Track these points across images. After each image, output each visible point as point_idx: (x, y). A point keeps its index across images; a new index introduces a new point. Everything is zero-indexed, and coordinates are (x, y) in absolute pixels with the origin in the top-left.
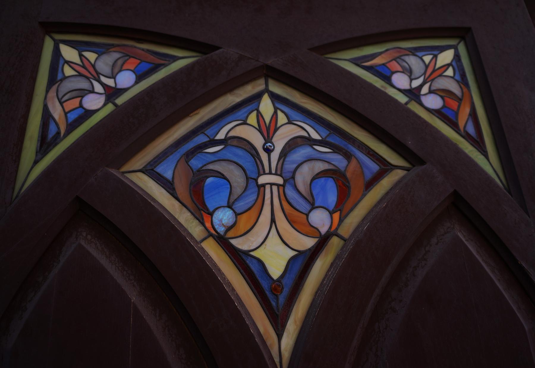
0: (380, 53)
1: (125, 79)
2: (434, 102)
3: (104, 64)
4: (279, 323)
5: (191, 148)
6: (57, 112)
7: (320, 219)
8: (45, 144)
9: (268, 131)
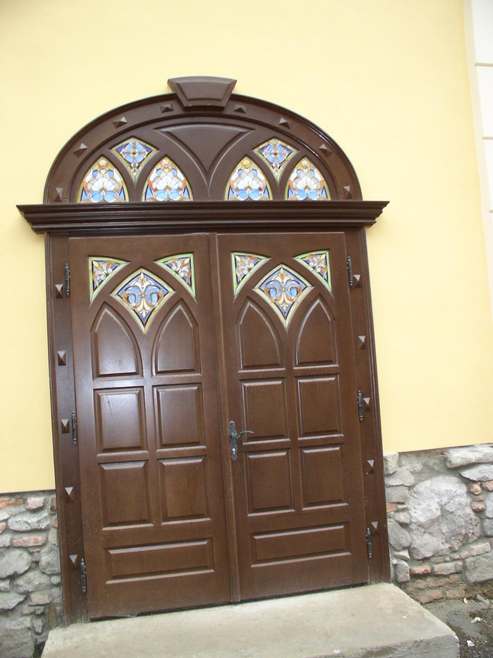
0: (170, 260)
2: (319, 270)
3: (247, 261)
4: (286, 318)
6: (239, 275)
8: (238, 283)
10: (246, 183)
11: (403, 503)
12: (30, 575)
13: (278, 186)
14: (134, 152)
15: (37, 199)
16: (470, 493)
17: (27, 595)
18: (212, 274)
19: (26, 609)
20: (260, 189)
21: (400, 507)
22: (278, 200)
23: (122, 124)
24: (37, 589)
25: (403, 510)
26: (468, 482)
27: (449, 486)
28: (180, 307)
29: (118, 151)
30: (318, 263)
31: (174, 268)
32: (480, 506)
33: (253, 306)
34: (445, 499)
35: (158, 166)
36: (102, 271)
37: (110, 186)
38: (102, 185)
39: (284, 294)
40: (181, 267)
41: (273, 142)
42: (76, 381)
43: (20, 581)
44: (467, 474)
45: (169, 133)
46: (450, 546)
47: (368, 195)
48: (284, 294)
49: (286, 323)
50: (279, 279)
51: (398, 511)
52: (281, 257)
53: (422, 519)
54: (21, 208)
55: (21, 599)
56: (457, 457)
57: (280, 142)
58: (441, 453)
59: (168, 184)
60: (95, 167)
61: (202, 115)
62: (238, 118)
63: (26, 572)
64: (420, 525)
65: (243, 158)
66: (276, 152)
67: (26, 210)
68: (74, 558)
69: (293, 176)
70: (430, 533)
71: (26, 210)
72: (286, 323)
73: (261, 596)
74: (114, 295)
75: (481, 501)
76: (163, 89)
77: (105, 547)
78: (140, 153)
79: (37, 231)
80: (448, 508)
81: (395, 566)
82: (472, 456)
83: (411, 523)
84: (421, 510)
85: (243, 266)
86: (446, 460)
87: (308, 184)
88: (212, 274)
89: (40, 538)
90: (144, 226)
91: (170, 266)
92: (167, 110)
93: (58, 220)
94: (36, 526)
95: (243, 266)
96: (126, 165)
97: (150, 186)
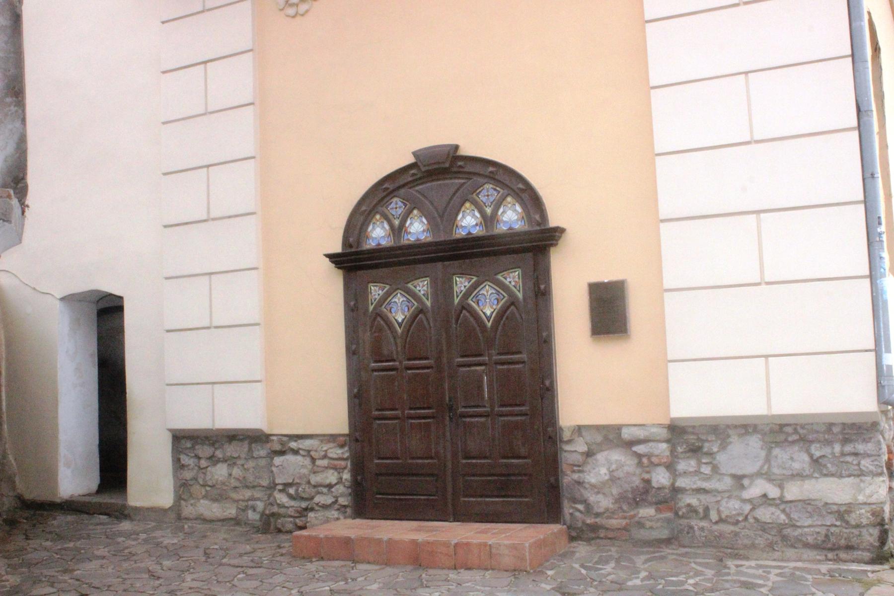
0: (415, 282)
1: (466, 284)
2: (513, 283)
5: (389, 303)
7: (494, 307)
9: (487, 292)
10: (468, 222)
11: (579, 466)
12: (337, 486)
13: (489, 220)
14: (396, 206)
15: (337, 248)
16: (640, 464)
17: (336, 497)
18: (443, 289)
19: (336, 506)
20: (477, 225)
21: (575, 468)
22: (442, 238)
23: (387, 189)
24: (342, 495)
25: (579, 471)
26: (639, 456)
27: (616, 456)
28: (512, 307)
29: (387, 208)
30: (513, 278)
31: (418, 288)
32: (646, 476)
33: (467, 314)
34: (614, 467)
35: (411, 216)
36: (376, 291)
37: (473, 222)
38: (378, 234)
39: (488, 304)
40: (422, 287)
41: (487, 186)
42: (175, 382)
43: (333, 490)
44: (640, 449)
45: (417, 191)
46: (746, 495)
47: (553, 222)
48: (488, 304)
49: (489, 325)
50: (396, 300)
51: (574, 471)
52: (398, 285)
53: (593, 481)
54: (328, 256)
55: (333, 500)
56: (626, 434)
57: (491, 186)
58: (618, 428)
59: (417, 229)
60: (374, 220)
61: (443, 172)
62: (458, 173)
63: (336, 484)
64: (593, 486)
65: (463, 204)
66: (488, 193)
67: (332, 257)
68: (359, 478)
69: (501, 211)
70: (604, 494)
71: (332, 257)
72: (489, 325)
73: (420, 517)
74: (383, 308)
75: (648, 472)
76: (411, 160)
77: (826, 459)
78: (400, 207)
79: (339, 268)
80: (615, 474)
81: (571, 514)
82: (641, 433)
83: (584, 482)
84: (597, 472)
85: (461, 284)
86: (620, 435)
87: (511, 217)
88: (443, 289)
89: (343, 463)
90: (400, 260)
91: (415, 287)
92: (413, 175)
93: (353, 262)
94: (341, 456)
95: (461, 284)
96: (391, 217)
97: (406, 230)
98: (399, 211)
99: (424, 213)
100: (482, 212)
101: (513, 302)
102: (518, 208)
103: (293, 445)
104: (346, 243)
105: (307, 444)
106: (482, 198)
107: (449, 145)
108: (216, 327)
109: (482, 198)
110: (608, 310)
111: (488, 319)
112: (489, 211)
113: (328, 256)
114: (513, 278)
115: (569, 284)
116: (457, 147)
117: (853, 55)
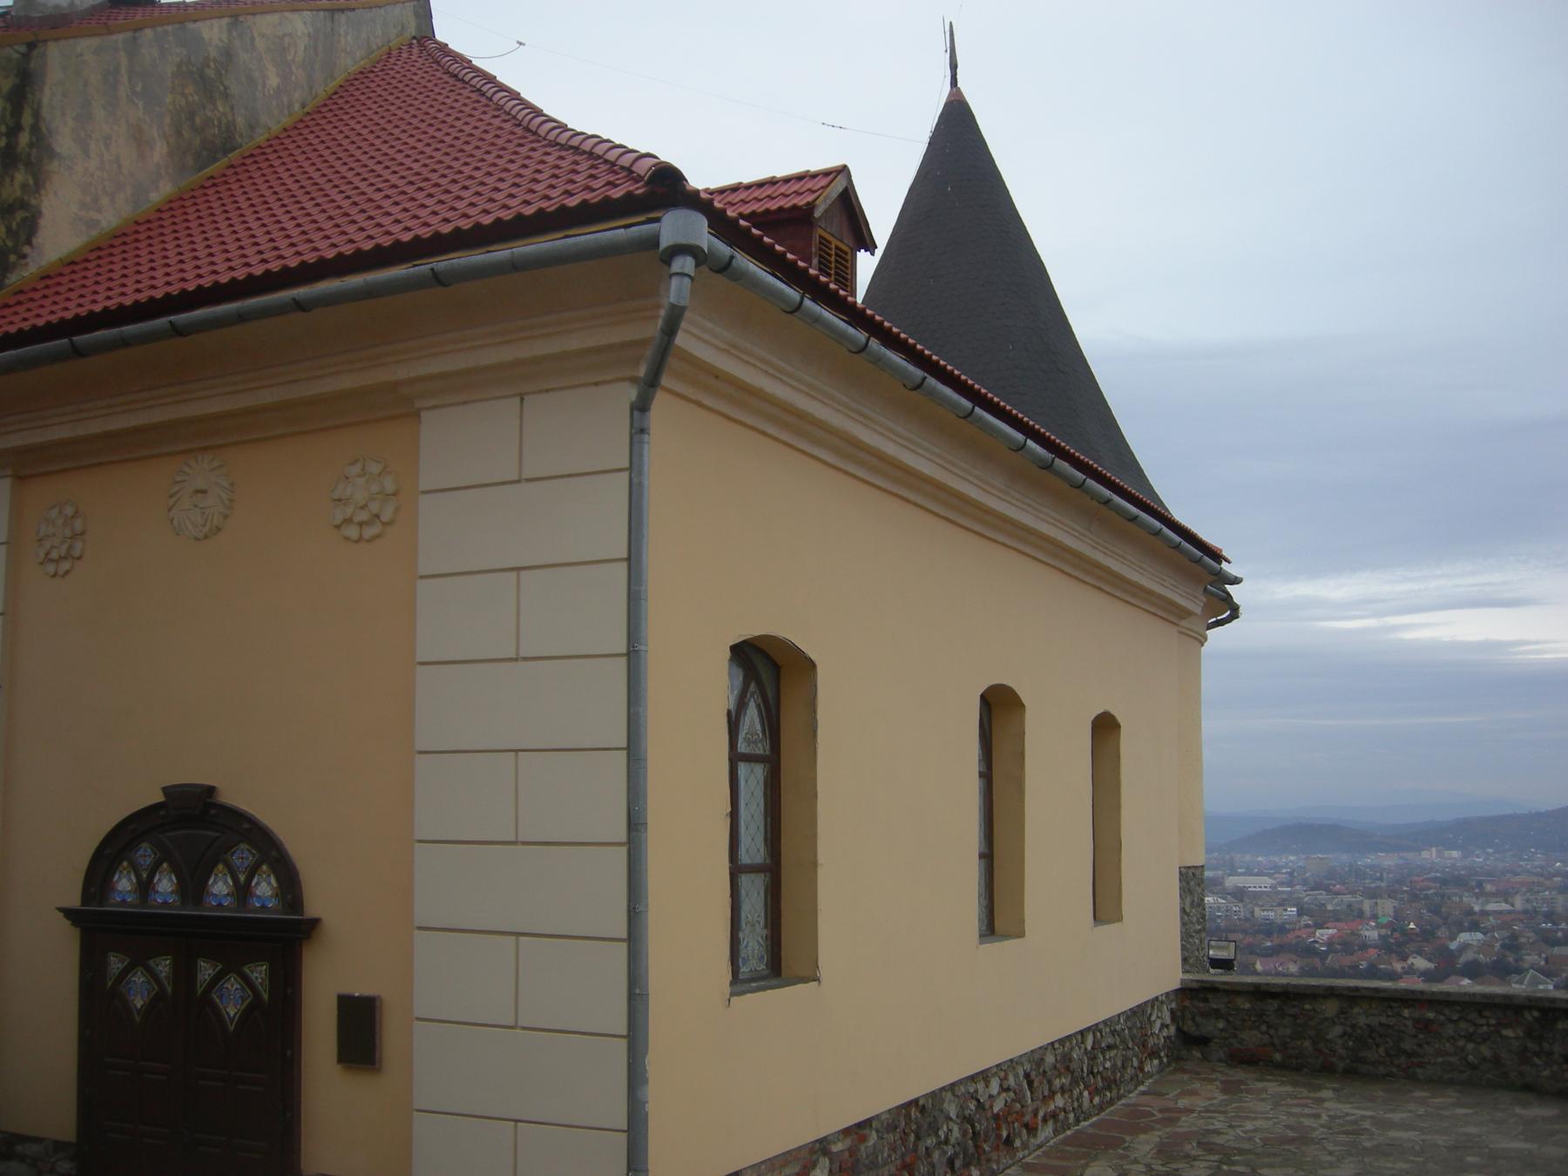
0: (157, 960)
14: (145, 854)
18: (184, 973)
30: (259, 973)
45: (1143, 1093)
49: (232, 1028)
54: (60, 910)
61: (193, 824)
67: (68, 913)
71: (68, 913)
76: (160, 798)
88: (184, 973)
95: (206, 970)
98: (149, 861)
99: (176, 870)
100: (138, 876)
101: (257, 1001)
102: (273, 881)
103: (19, 1148)
104: (86, 896)
105: (34, 1149)
106: (236, 860)
107: (201, 786)
108: (524, 843)
109: (236, 860)
110: (361, 1030)
111: (232, 1020)
112: (242, 878)
113: (60, 910)
114: (259, 973)
115: (325, 981)
116: (211, 790)
117: (628, 748)
